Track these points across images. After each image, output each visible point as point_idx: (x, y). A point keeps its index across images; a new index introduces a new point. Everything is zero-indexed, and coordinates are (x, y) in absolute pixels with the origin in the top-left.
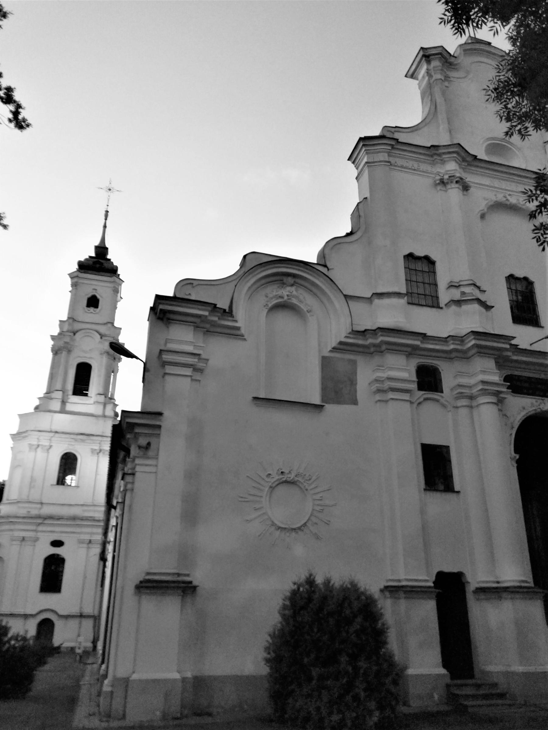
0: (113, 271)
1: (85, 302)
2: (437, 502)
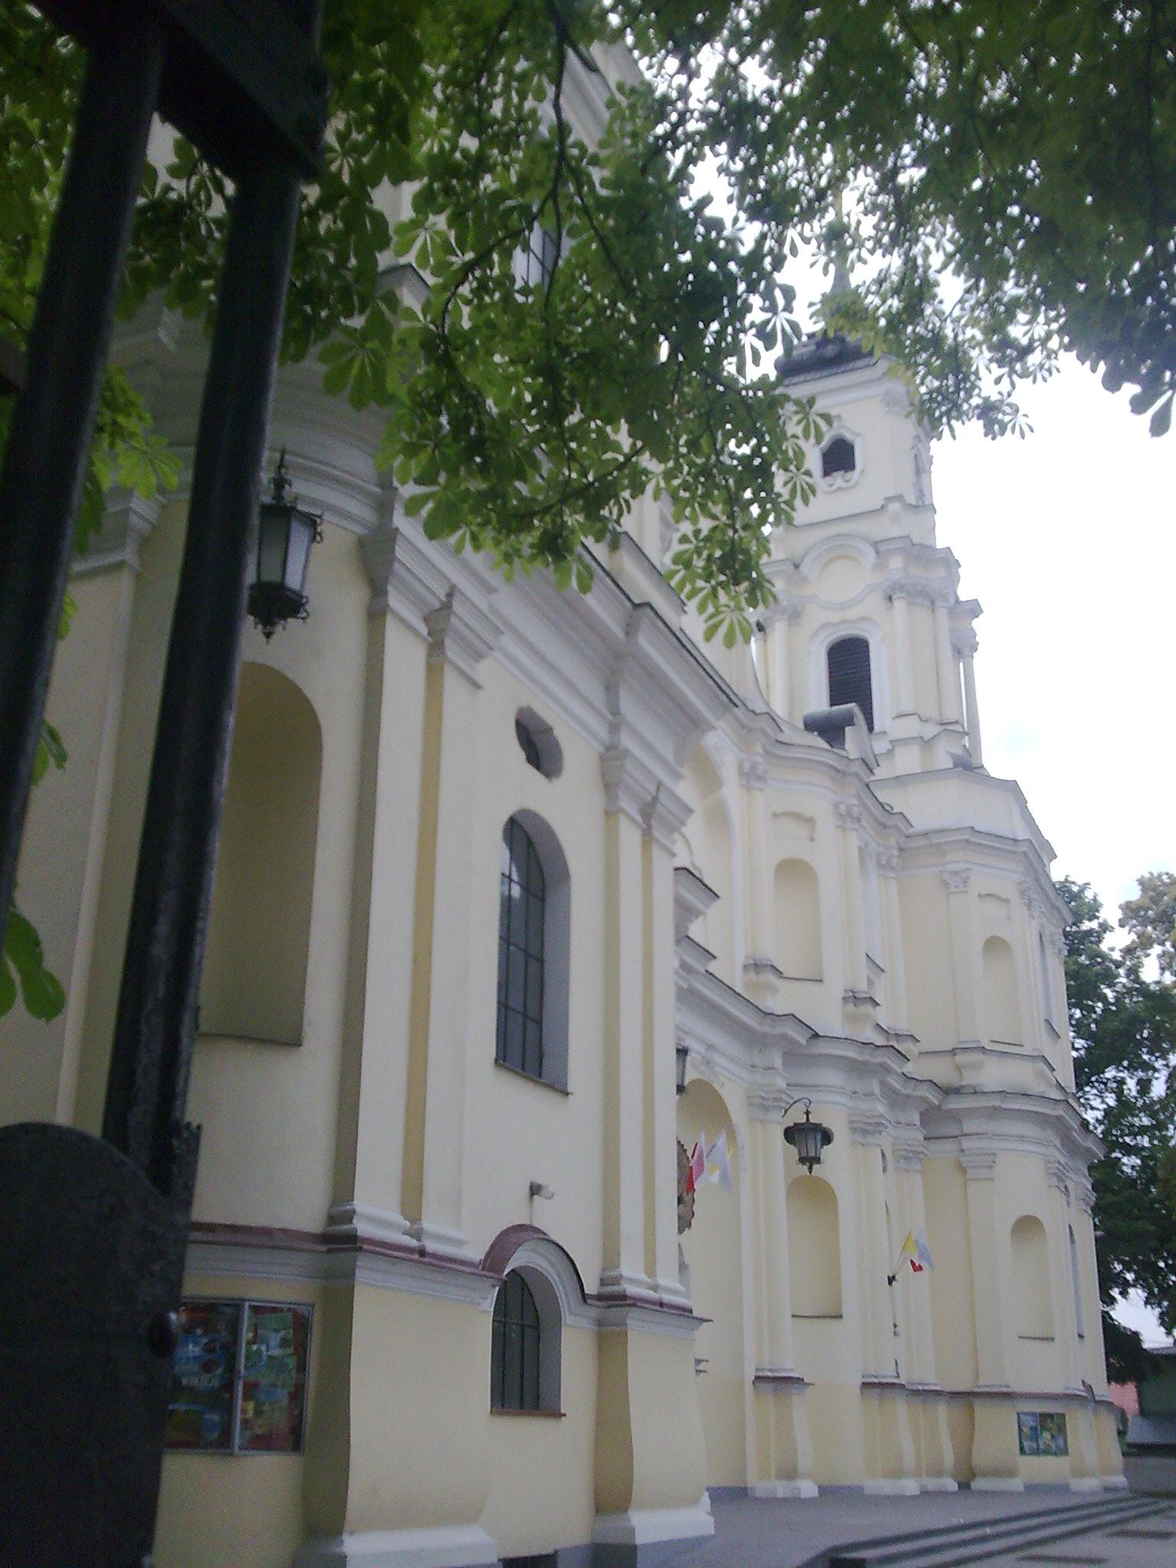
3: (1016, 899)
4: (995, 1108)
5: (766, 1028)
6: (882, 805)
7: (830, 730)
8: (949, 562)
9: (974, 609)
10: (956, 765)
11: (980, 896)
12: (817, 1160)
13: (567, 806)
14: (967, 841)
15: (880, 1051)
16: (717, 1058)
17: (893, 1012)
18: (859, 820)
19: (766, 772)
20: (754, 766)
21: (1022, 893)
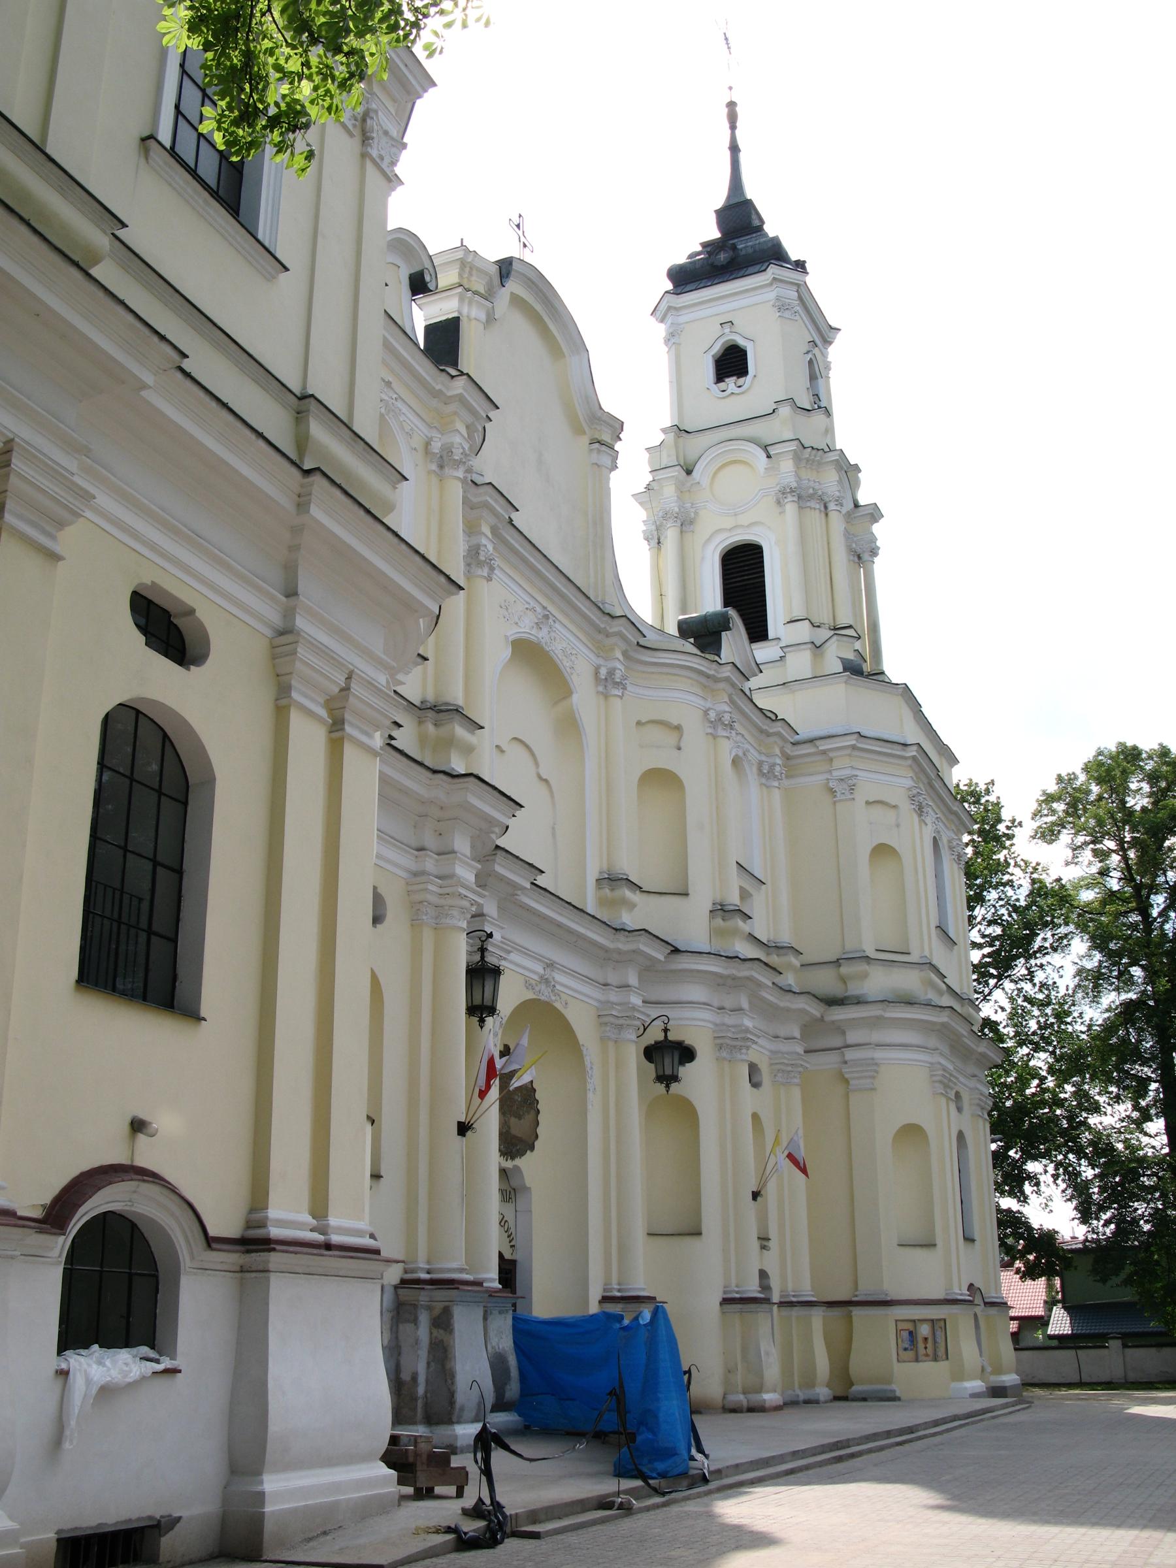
0: (775, 253)
1: (708, 369)
2: (126, 1034)
3: (906, 807)
4: (878, 1018)
5: (622, 944)
6: (761, 709)
7: (704, 635)
8: (849, 472)
9: (874, 514)
10: (845, 670)
11: (868, 803)
12: (675, 1078)
13: (209, 705)
14: (854, 747)
15: (748, 964)
16: (559, 977)
17: (769, 919)
18: (732, 728)
19: (624, 678)
20: (611, 673)
21: (912, 798)
